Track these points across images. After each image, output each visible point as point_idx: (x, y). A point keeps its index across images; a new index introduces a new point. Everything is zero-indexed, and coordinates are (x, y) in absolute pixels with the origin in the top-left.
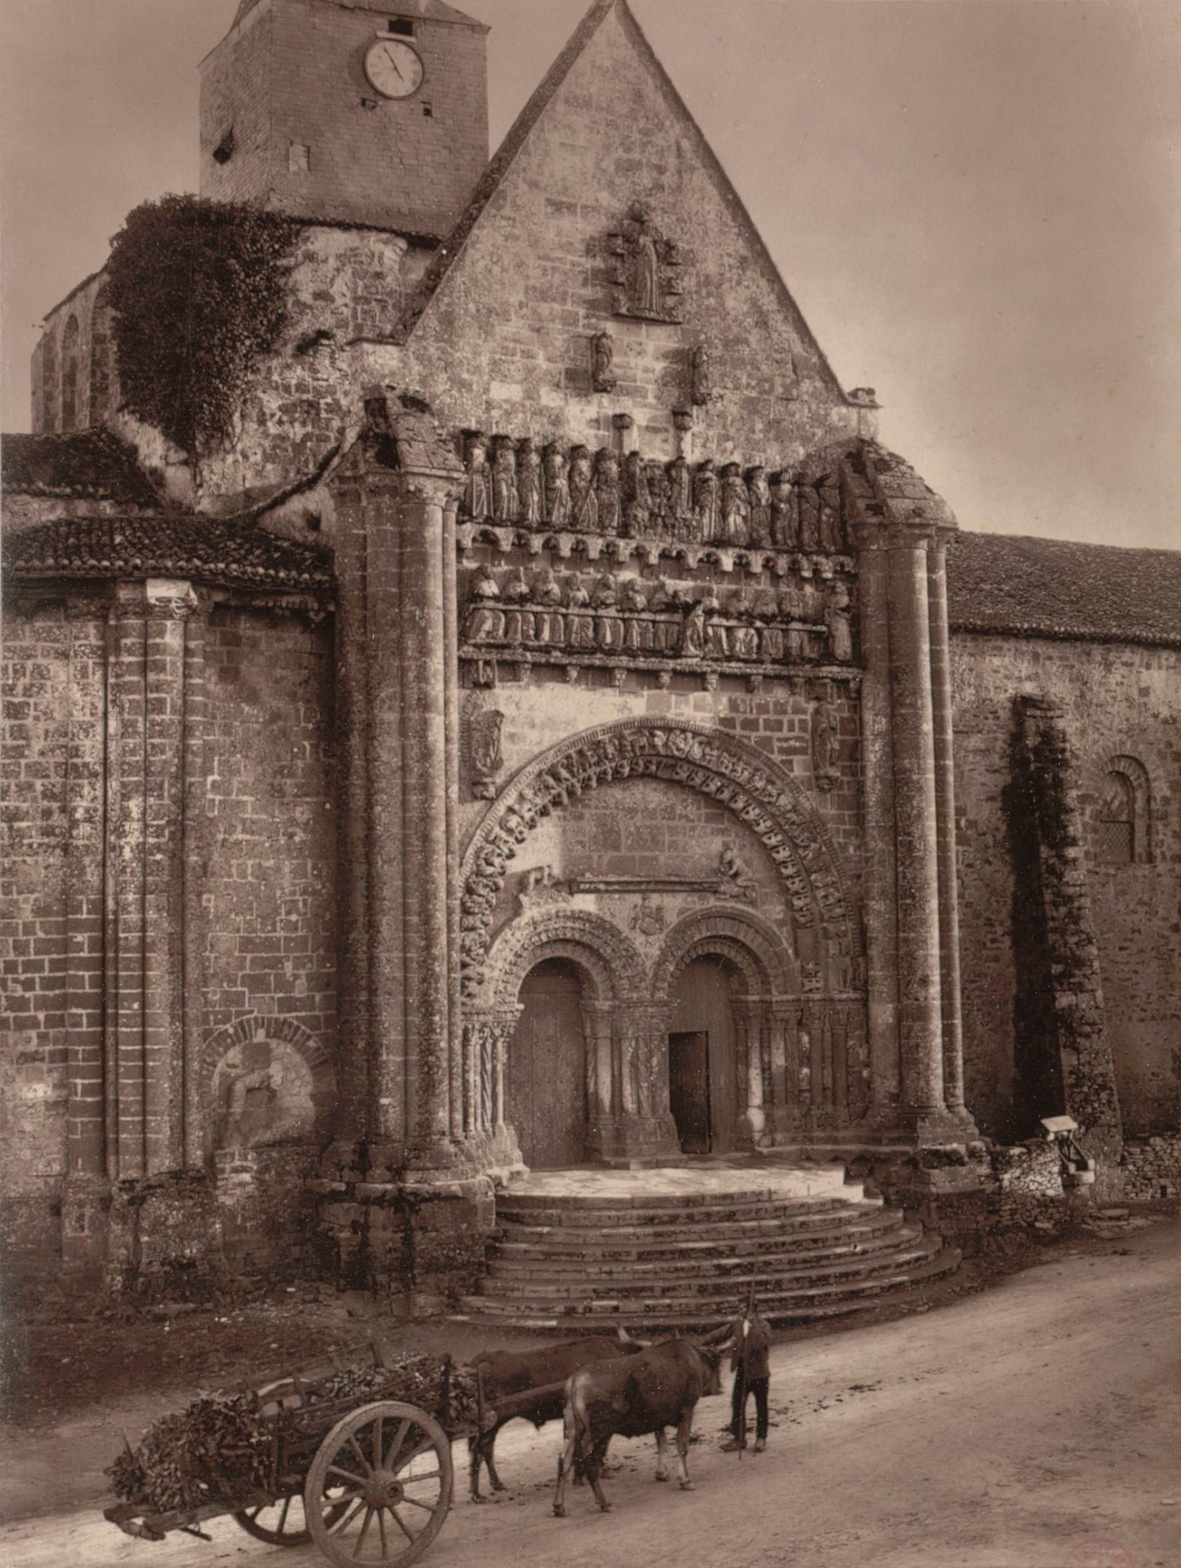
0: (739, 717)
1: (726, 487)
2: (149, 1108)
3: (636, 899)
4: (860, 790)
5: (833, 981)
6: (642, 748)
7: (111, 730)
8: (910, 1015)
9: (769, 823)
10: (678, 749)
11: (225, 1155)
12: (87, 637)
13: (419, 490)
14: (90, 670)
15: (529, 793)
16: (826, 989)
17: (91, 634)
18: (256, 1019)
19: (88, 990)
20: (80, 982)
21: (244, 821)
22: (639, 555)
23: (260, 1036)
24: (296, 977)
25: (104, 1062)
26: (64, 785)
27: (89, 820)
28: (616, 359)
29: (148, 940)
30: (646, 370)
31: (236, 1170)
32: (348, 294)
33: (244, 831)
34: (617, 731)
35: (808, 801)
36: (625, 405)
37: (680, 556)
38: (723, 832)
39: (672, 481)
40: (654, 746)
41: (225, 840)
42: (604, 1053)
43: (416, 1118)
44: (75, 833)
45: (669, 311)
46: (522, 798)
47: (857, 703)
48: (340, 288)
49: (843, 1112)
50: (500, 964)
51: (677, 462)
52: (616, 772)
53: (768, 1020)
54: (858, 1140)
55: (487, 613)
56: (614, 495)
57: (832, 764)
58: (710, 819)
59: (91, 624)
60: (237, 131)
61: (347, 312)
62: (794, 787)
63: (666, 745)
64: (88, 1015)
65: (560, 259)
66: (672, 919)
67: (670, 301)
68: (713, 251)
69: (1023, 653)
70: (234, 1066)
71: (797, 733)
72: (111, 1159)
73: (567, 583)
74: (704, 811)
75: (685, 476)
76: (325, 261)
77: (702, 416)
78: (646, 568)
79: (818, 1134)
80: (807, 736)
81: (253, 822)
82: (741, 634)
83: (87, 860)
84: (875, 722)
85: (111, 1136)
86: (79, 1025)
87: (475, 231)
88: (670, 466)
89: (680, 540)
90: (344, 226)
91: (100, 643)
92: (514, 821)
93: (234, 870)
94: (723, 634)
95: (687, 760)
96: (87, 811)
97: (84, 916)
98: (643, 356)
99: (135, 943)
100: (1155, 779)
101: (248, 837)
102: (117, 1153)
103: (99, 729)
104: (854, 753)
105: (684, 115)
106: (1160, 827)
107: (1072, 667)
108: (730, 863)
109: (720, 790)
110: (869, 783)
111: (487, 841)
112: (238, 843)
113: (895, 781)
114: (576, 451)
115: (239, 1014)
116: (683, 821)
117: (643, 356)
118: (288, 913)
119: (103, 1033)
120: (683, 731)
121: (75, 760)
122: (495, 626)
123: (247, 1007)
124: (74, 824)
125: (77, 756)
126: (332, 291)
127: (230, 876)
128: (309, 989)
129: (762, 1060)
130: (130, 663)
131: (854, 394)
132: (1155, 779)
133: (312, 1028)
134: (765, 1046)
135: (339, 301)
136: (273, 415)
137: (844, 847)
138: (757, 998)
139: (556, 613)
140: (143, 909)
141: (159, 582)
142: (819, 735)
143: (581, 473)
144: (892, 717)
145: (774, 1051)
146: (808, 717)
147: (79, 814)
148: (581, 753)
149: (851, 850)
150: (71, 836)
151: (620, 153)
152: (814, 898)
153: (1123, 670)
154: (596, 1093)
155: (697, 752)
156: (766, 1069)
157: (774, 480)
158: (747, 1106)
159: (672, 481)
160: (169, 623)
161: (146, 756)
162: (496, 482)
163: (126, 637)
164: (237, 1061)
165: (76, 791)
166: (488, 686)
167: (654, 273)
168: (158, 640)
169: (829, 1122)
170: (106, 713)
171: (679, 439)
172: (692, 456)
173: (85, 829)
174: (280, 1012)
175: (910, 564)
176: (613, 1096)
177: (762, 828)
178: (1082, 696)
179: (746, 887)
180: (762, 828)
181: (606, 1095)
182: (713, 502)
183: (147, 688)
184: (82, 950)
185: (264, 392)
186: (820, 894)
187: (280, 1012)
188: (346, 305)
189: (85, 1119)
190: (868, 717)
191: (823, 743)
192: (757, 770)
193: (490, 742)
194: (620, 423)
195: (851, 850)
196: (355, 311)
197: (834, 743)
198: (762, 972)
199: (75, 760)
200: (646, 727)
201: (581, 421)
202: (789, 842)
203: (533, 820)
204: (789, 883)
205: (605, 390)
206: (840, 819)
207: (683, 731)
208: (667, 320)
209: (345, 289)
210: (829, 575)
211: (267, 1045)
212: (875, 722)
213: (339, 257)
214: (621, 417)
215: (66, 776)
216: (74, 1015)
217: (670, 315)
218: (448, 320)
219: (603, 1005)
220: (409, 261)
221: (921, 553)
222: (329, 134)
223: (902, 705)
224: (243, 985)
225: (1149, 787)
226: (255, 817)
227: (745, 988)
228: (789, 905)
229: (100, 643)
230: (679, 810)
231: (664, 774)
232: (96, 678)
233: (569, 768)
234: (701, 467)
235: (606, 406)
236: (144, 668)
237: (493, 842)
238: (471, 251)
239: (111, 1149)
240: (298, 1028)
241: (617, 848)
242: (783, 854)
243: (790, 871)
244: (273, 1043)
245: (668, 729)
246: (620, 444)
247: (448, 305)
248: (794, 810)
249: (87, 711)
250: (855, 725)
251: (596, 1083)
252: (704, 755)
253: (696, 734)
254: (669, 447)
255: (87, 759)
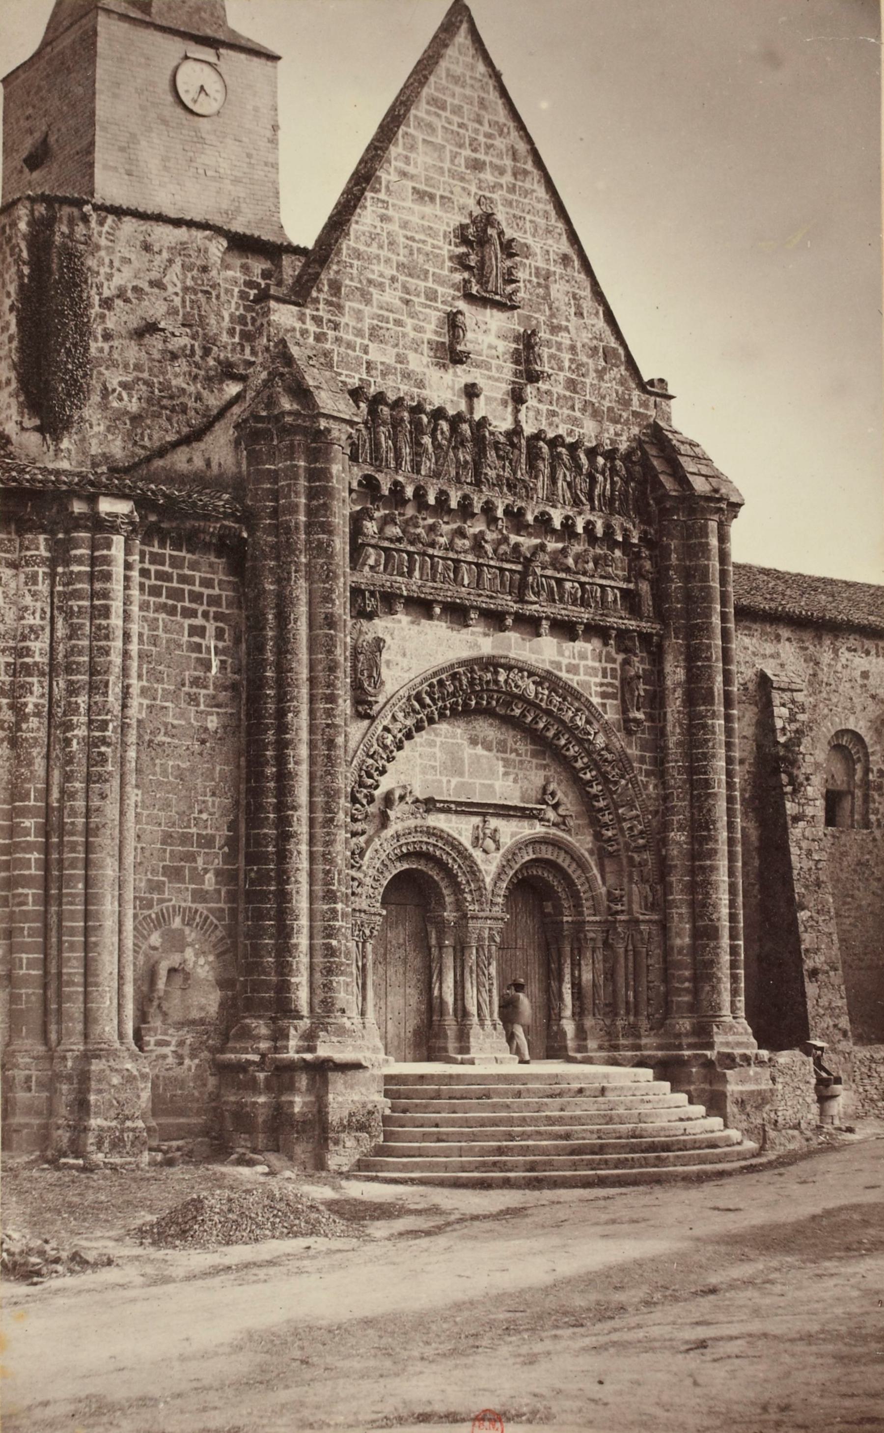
0: (565, 662)
1: (556, 458)
2: (91, 979)
3: (476, 820)
4: (660, 733)
5: (635, 907)
6: (488, 682)
7: (59, 634)
8: (705, 933)
9: (586, 760)
10: (517, 686)
11: (149, 1029)
12: (37, 549)
13: (328, 430)
14: (40, 578)
15: (400, 715)
16: (630, 912)
17: (41, 546)
18: (174, 907)
19: (33, 872)
20: (27, 864)
21: (166, 725)
22: (488, 509)
23: (177, 923)
24: (206, 871)
25: (46, 938)
26: (12, 683)
27: (38, 714)
28: (469, 335)
29: (92, 826)
30: (490, 347)
31: (159, 1043)
32: (179, 285)
33: (166, 734)
34: (469, 664)
35: (619, 741)
36: (475, 376)
37: (521, 512)
38: (545, 767)
39: (513, 445)
40: (496, 682)
41: (151, 741)
42: (449, 961)
43: (320, 995)
44: (24, 726)
45: (510, 297)
46: (394, 718)
47: (657, 657)
48: (174, 278)
49: (644, 1024)
50: (371, 872)
51: (517, 431)
52: (466, 704)
53: (579, 940)
54: (659, 1048)
55: (371, 550)
56: (465, 455)
57: (638, 709)
58: (535, 754)
59: (42, 538)
60: (52, 139)
61: (177, 301)
62: (606, 728)
63: (506, 681)
64: (34, 895)
65: (424, 242)
66: (507, 841)
67: (509, 289)
68: (543, 247)
69: (767, 634)
70: (155, 948)
71: (609, 680)
72: (53, 1027)
73: (432, 529)
74: (530, 747)
75: (523, 442)
76: (160, 252)
77: (535, 392)
78: (492, 520)
79: (622, 1041)
80: (617, 683)
81: (174, 727)
82: (568, 585)
83: (35, 752)
84: (675, 673)
85: (54, 1006)
86: (25, 903)
87: (358, 210)
88: (509, 434)
89: (521, 498)
90: (177, 223)
91: (48, 554)
92: (389, 740)
93: (158, 769)
94: (553, 583)
95: (522, 698)
96: (36, 706)
97: (32, 803)
98: (489, 333)
99: (80, 828)
100: (873, 753)
101: (169, 740)
102: (59, 1022)
103: (48, 630)
104: (656, 701)
105: (521, 127)
106: (876, 797)
107: (807, 649)
108: (553, 794)
109: (546, 728)
110: (669, 728)
111: (368, 756)
112: (161, 744)
113: (690, 726)
114: (439, 414)
115: (161, 901)
116: (513, 756)
117: (489, 333)
118: (200, 812)
119: (46, 912)
120: (521, 670)
121: (27, 660)
122: (377, 561)
123: (166, 896)
124: (24, 718)
125: (28, 655)
126: (165, 281)
127: (154, 774)
128: (217, 883)
129: (572, 975)
130: (79, 572)
131: (651, 383)
132: (873, 753)
133: (218, 919)
134: (576, 965)
135: (171, 290)
136: (114, 390)
137: (646, 787)
138: (570, 919)
139: (424, 554)
140: (87, 798)
141: (108, 499)
142: (627, 683)
143: (442, 433)
144: (689, 670)
145: (584, 968)
146: (617, 666)
147: (30, 709)
148: (454, 677)
149: (651, 787)
150: (20, 730)
151: (467, 152)
152: (621, 830)
153: (848, 655)
154: (441, 996)
155: (531, 690)
156: (577, 985)
157: (592, 453)
158: (560, 1018)
159: (513, 445)
160: (115, 538)
161: (91, 658)
162: (376, 433)
163: (76, 548)
164: (158, 944)
165: (27, 689)
166: (370, 616)
167: (498, 263)
168: (105, 552)
169: (633, 1031)
170: (52, 618)
171: (517, 411)
172: (529, 429)
173: (34, 722)
174: (193, 901)
175: (704, 532)
176: (456, 1000)
177: (579, 764)
178: (815, 675)
179: (564, 817)
180: (579, 764)
181: (450, 999)
182: (544, 467)
183: (94, 595)
184: (29, 835)
185: (107, 368)
186: (626, 825)
187: (193, 901)
188: (176, 294)
189: (30, 991)
190: (668, 668)
191: (632, 691)
192: (578, 710)
193: (374, 665)
194: (471, 392)
195: (651, 787)
196: (184, 301)
197: (642, 688)
198: (575, 895)
199: (27, 660)
200: (491, 664)
201: (442, 389)
202: (600, 779)
203: (401, 741)
204: (599, 816)
205: (462, 362)
206: (642, 760)
207: (521, 670)
208: (507, 306)
209: (175, 280)
210: (635, 541)
211: (182, 931)
212: (675, 673)
213: (170, 249)
214: (474, 385)
215: (14, 675)
216: (21, 895)
217: (511, 300)
218: (336, 287)
219: (449, 915)
220: (229, 259)
221: (713, 525)
222: (144, 143)
223: (699, 658)
224: (164, 875)
225: (867, 761)
226: (176, 722)
227: (558, 910)
228: (598, 836)
229: (48, 554)
230: (510, 742)
231: (501, 711)
232: (43, 587)
233: (430, 694)
234: (538, 436)
235: (462, 376)
236: (92, 577)
237: (372, 757)
238: (354, 226)
239: (53, 1019)
240: (207, 918)
241: (461, 774)
242: (595, 789)
243: (602, 804)
244: (187, 930)
245: (509, 668)
246: (471, 410)
247: (337, 272)
248: (606, 748)
249: (38, 615)
250: (657, 676)
251: (440, 988)
252: (537, 693)
253: (531, 674)
254: (510, 419)
255: (38, 659)
